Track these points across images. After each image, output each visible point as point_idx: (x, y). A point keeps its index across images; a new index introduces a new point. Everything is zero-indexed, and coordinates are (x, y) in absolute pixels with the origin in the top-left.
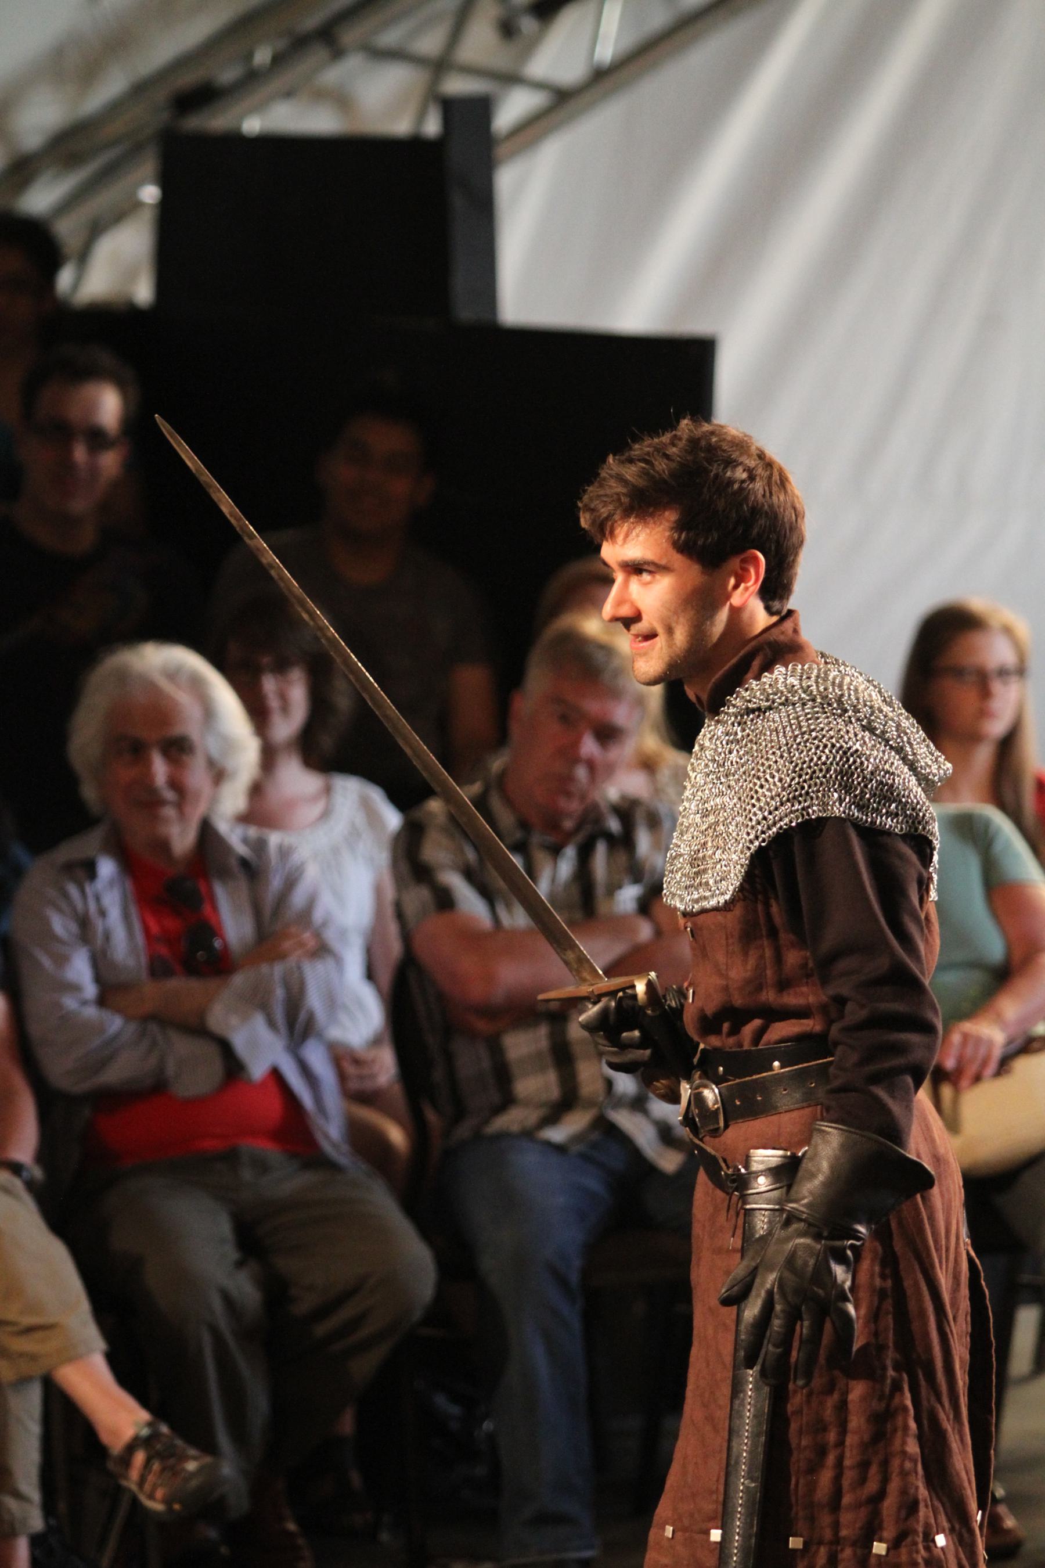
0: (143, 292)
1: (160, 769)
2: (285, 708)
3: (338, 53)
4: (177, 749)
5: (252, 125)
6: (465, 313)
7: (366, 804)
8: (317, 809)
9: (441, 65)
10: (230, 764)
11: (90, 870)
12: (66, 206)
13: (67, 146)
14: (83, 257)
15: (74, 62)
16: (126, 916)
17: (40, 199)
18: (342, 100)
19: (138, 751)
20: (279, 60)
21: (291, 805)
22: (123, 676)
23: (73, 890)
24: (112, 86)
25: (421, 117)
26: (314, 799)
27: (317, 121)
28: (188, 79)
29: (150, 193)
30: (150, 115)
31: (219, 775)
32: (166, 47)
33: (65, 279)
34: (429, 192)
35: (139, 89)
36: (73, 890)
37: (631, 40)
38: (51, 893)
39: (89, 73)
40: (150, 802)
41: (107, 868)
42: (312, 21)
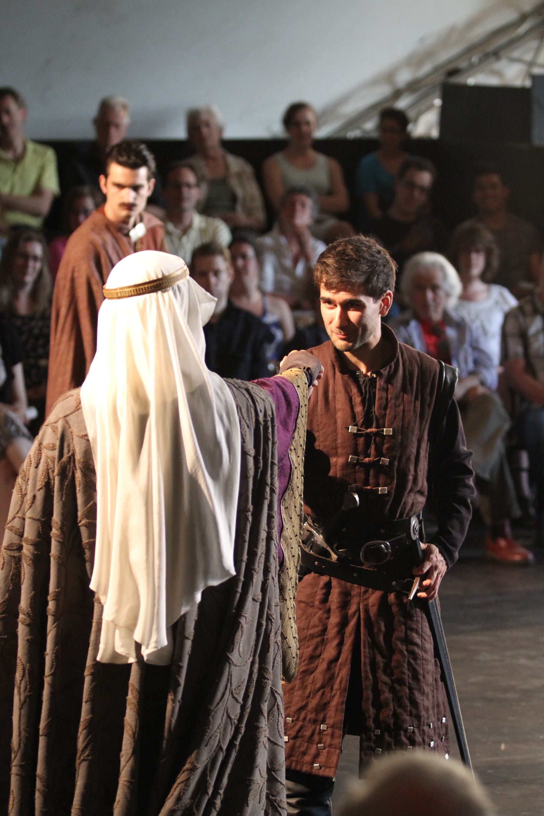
0: (435, 133)
1: (430, 295)
4: (435, 288)
5: (471, 81)
7: (502, 295)
9: (531, 64)
12: (412, 106)
13: (412, 86)
14: (416, 120)
15: (415, 60)
17: (402, 104)
18: (499, 74)
20: (481, 61)
22: (417, 264)
24: (427, 68)
25: (524, 80)
27: (492, 81)
28: (450, 67)
29: (438, 102)
30: (439, 78)
31: (448, 295)
32: (444, 56)
33: (410, 127)
35: (436, 69)
40: (425, 306)
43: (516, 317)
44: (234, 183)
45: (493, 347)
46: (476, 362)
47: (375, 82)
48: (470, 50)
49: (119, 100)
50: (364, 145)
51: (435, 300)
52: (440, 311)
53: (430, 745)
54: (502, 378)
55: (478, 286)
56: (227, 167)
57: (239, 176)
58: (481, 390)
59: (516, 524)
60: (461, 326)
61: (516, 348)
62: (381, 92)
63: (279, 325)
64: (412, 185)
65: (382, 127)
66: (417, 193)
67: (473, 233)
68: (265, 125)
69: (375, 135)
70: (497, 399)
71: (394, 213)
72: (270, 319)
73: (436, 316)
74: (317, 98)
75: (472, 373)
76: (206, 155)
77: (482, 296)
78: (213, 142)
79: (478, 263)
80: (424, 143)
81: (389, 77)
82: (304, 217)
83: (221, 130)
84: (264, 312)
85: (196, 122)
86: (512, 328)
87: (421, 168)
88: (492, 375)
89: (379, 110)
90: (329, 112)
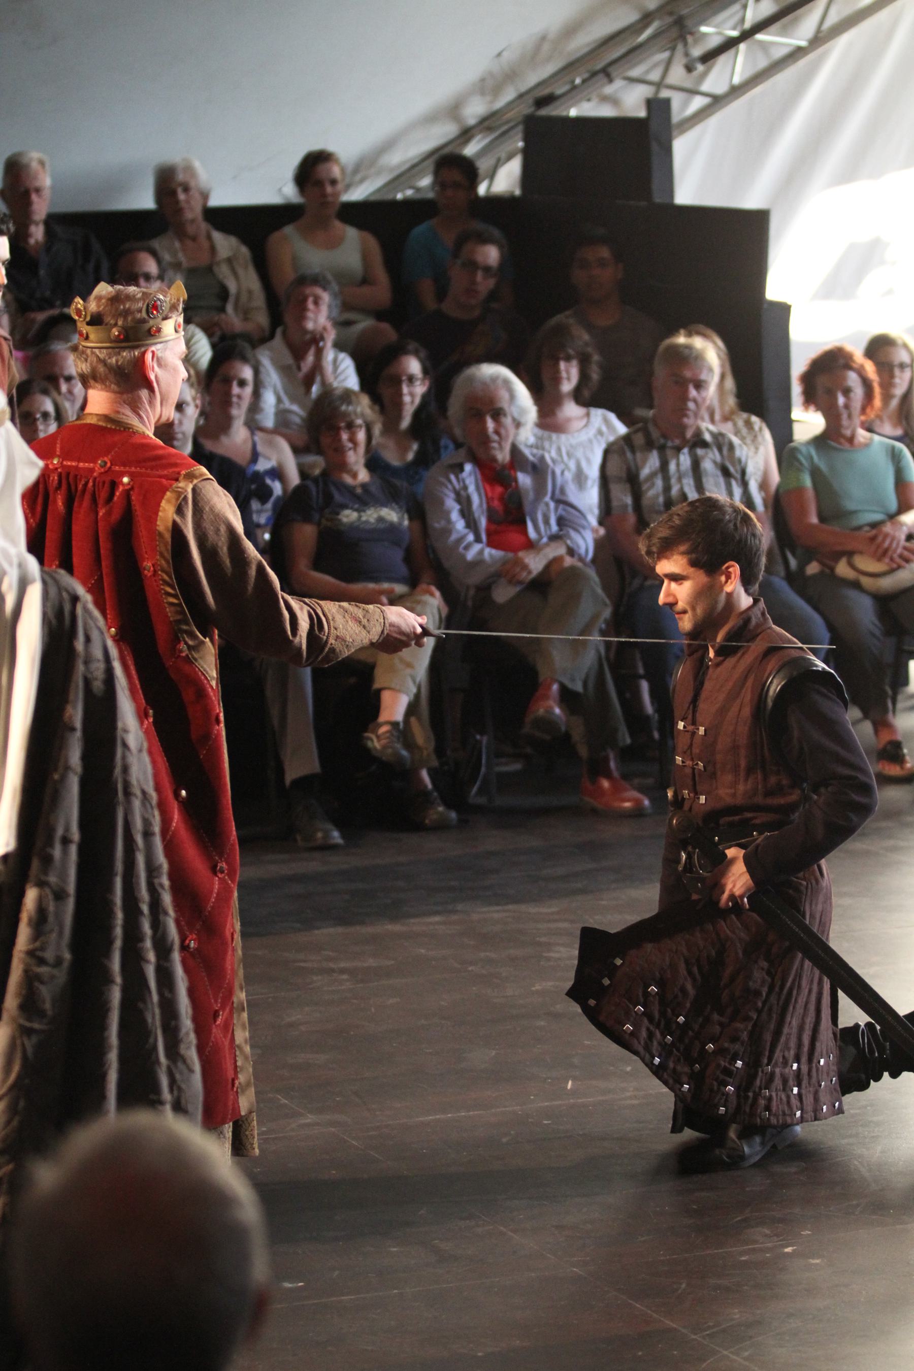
0: (518, 192)
1: (490, 425)
2: (569, 379)
3: (611, 80)
4: (498, 414)
5: (573, 113)
6: (658, 199)
7: (606, 421)
8: (584, 421)
9: (659, 85)
10: (523, 420)
11: (460, 468)
13: (487, 123)
14: (492, 176)
15: (488, 85)
16: (478, 488)
17: (470, 150)
18: (613, 101)
19: (479, 417)
21: (569, 420)
22: (471, 379)
23: (452, 477)
24: (508, 95)
26: (582, 418)
27: (606, 111)
28: (546, 91)
30: (526, 109)
31: (518, 425)
32: (532, 79)
33: (482, 190)
34: (643, 142)
35: (521, 96)
36: (452, 477)
37: (749, 73)
38: (443, 480)
39: (496, 90)
40: (485, 440)
41: (468, 467)
42: (599, 66)
43: (622, 453)
44: (223, 272)
45: (589, 499)
46: (561, 521)
47: (431, 118)
48: (570, 67)
49: (34, 156)
50: (417, 209)
51: (497, 432)
52: (507, 448)
53: (792, 1066)
54: (599, 544)
55: (571, 410)
56: (213, 249)
57: (229, 261)
58: (568, 561)
59: (626, 755)
60: (538, 470)
61: (623, 498)
62: (440, 134)
63: (277, 473)
64: (472, 265)
65: (440, 182)
66: (480, 276)
67: (561, 331)
68: (274, 187)
69: (431, 195)
70: (592, 573)
71: (448, 307)
72: (262, 466)
73: (503, 456)
74: (346, 147)
75: (554, 538)
76: (181, 233)
77: (577, 424)
78: (193, 212)
79: (569, 376)
80: (496, 202)
81: (453, 110)
82: (320, 316)
83: (205, 196)
84: (255, 456)
85: (168, 183)
86: (614, 469)
87: (485, 240)
88: (585, 541)
89: (436, 156)
90: (365, 165)
